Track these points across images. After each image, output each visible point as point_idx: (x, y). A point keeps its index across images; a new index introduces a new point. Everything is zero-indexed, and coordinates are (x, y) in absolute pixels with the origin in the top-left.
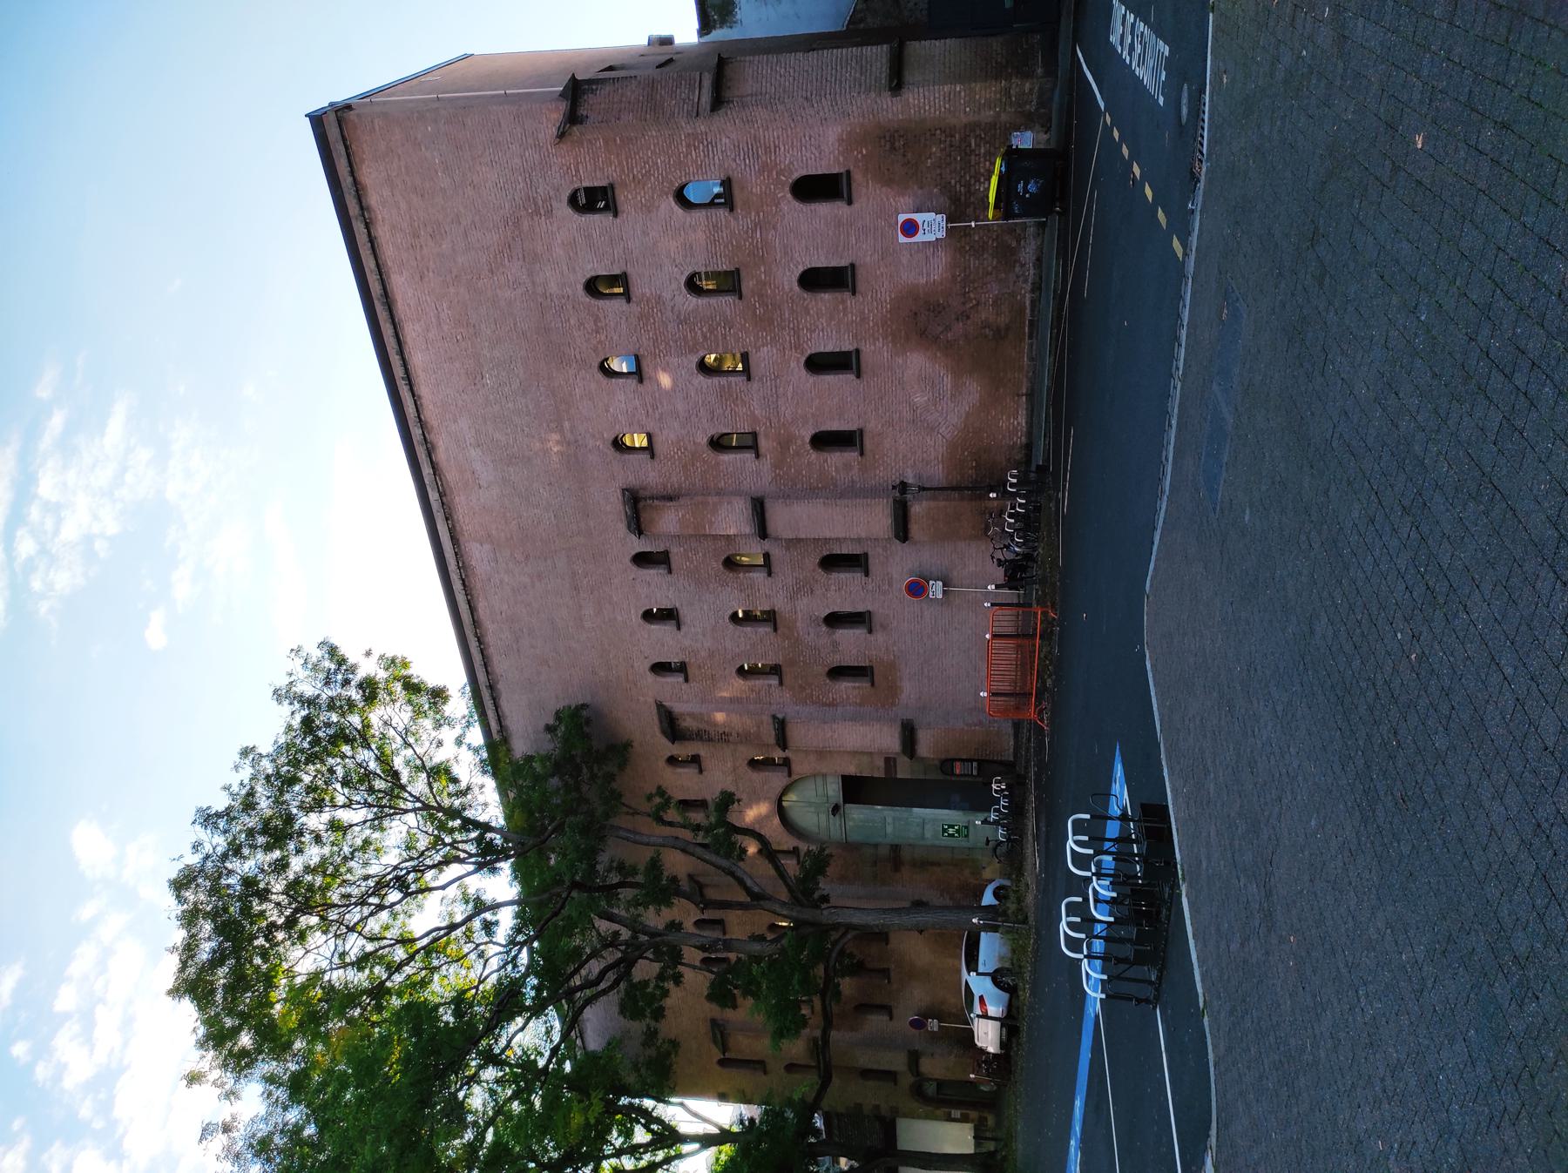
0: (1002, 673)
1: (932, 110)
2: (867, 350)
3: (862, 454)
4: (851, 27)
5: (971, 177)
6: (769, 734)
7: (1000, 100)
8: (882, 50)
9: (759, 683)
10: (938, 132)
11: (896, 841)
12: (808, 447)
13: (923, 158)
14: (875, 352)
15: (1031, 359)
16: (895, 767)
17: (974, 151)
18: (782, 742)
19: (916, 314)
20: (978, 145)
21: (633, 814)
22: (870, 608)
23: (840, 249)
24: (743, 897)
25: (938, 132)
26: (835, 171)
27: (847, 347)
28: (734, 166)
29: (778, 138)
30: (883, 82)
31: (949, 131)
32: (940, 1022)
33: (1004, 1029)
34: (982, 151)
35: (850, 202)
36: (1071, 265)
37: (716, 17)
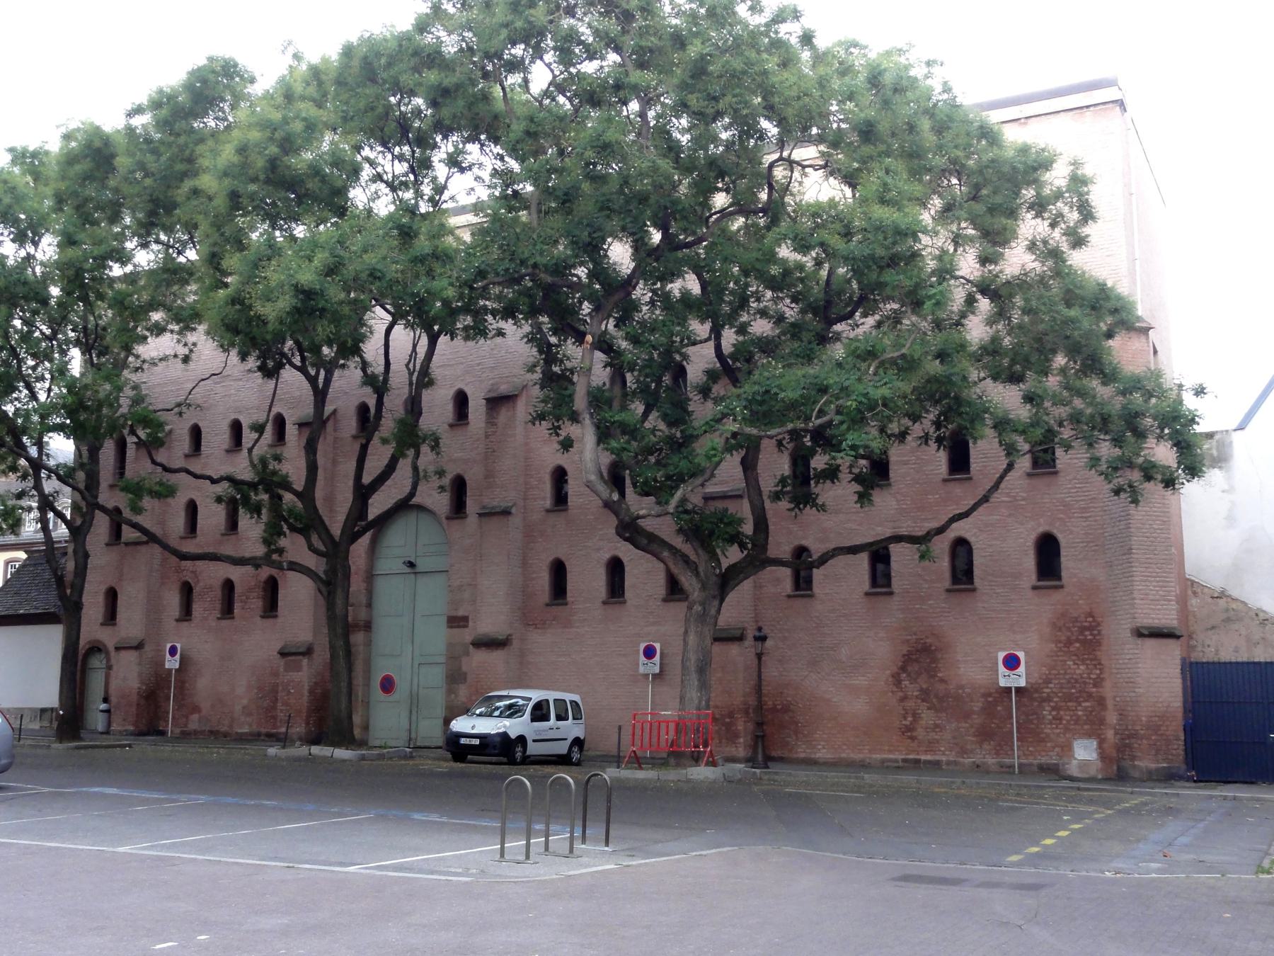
0: (655, 733)
1: (1118, 666)
2: (895, 602)
3: (789, 596)
4: (1189, 583)
5: (1056, 702)
6: (497, 500)
7: (1127, 729)
8: (1172, 619)
9: (662, 518)
10: (1098, 672)
11: (374, 626)
12: (797, 543)
13: (1074, 658)
14: (893, 611)
15: (883, 761)
16: (459, 627)
17: (1080, 705)
18: (488, 514)
19: (411, 565)
20: (1085, 709)
21: (416, 354)
22: (629, 602)
23: (990, 578)
24: (367, 479)
25: (1098, 672)
26: (1064, 574)
27: (896, 584)
28: (1070, 477)
29: (1095, 521)
30: (1145, 621)
31: (1098, 683)
32: (176, 670)
33: (476, 742)
34: (1080, 713)
35: (1035, 588)
36: (144, 848)
37: (834, 108)
